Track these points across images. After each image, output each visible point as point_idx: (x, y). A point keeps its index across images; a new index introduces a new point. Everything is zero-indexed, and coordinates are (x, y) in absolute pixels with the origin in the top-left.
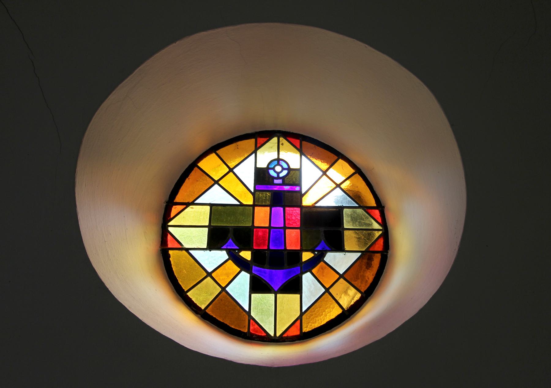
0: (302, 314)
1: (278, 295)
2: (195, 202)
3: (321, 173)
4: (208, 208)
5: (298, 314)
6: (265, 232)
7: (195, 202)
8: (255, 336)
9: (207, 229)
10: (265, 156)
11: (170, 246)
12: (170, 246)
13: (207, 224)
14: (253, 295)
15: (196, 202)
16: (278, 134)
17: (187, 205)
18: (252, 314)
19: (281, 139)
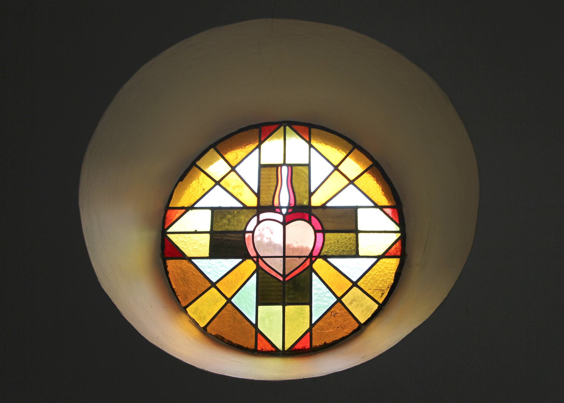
0: (312, 325)
1: (287, 307)
2: (195, 206)
3: (333, 168)
4: (209, 212)
5: (308, 326)
6: (289, 299)
7: (195, 206)
8: (259, 347)
9: (208, 236)
10: (272, 149)
11: (308, 346)
12: (308, 346)
13: (208, 229)
14: (259, 307)
15: (196, 206)
16: (285, 124)
17: (187, 209)
18: (260, 327)
19: (287, 128)
